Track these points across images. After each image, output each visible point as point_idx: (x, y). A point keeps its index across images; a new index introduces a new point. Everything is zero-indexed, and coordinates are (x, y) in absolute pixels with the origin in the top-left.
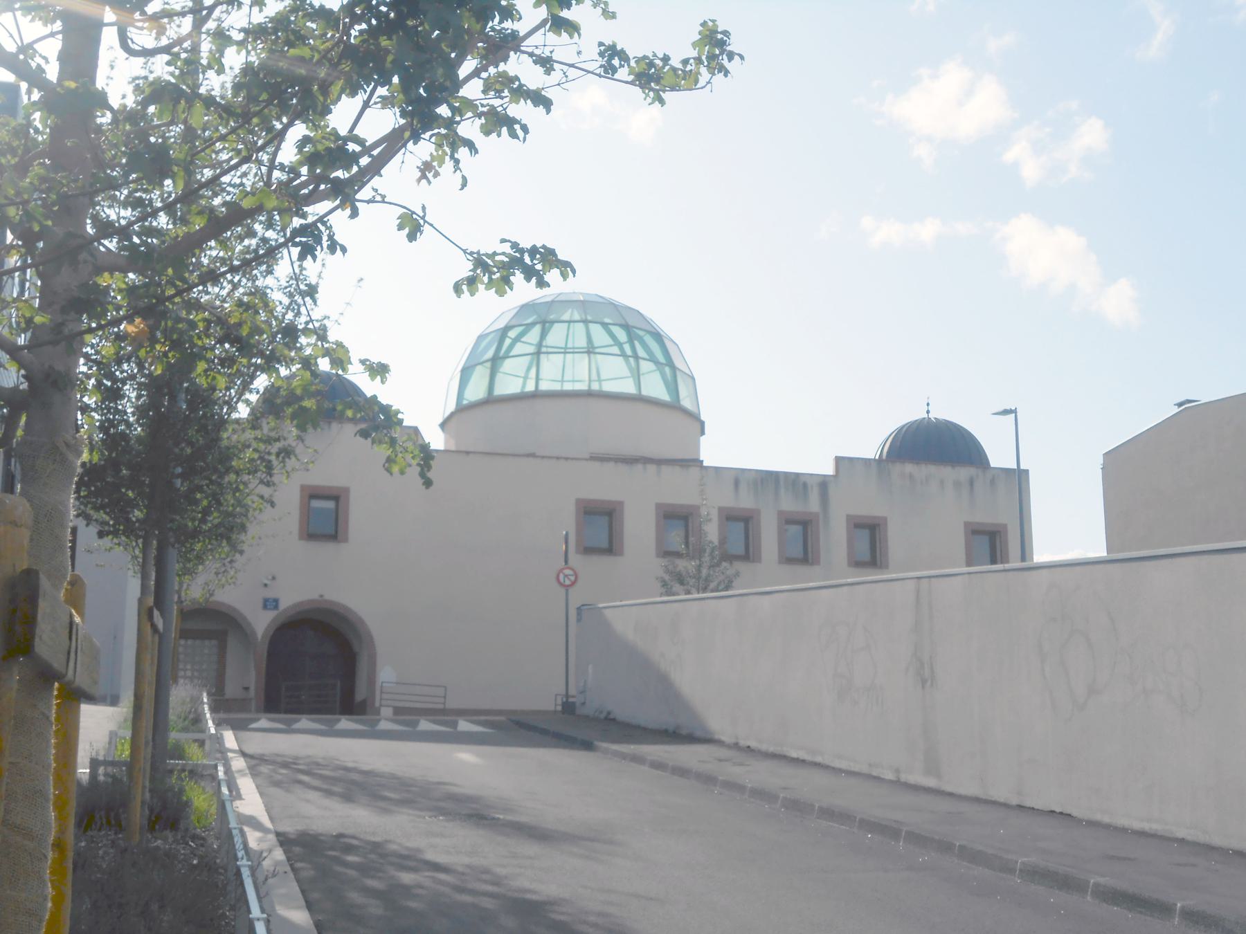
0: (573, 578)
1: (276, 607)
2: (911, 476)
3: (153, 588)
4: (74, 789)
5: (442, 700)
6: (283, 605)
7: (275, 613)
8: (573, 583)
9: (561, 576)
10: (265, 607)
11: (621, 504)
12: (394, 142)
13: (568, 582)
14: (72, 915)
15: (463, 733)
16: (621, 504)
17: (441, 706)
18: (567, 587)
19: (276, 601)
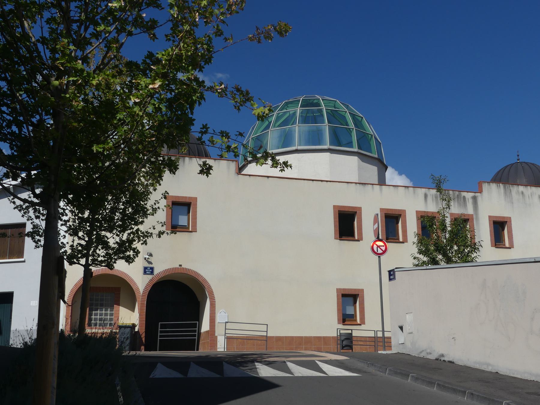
0: (383, 248)
1: (152, 273)
2: (522, 193)
3: (55, 385)
4: (55, 340)
5: (264, 328)
6: (156, 272)
7: (150, 277)
8: (384, 252)
9: (375, 247)
10: (145, 273)
11: (360, 209)
12: (82, 265)
13: (380, 251)
14: (58, 367)
15: (62, 274)
16: (360, 209)
17: (265, 334)
18: (379, 255)
19: (152, 269)
